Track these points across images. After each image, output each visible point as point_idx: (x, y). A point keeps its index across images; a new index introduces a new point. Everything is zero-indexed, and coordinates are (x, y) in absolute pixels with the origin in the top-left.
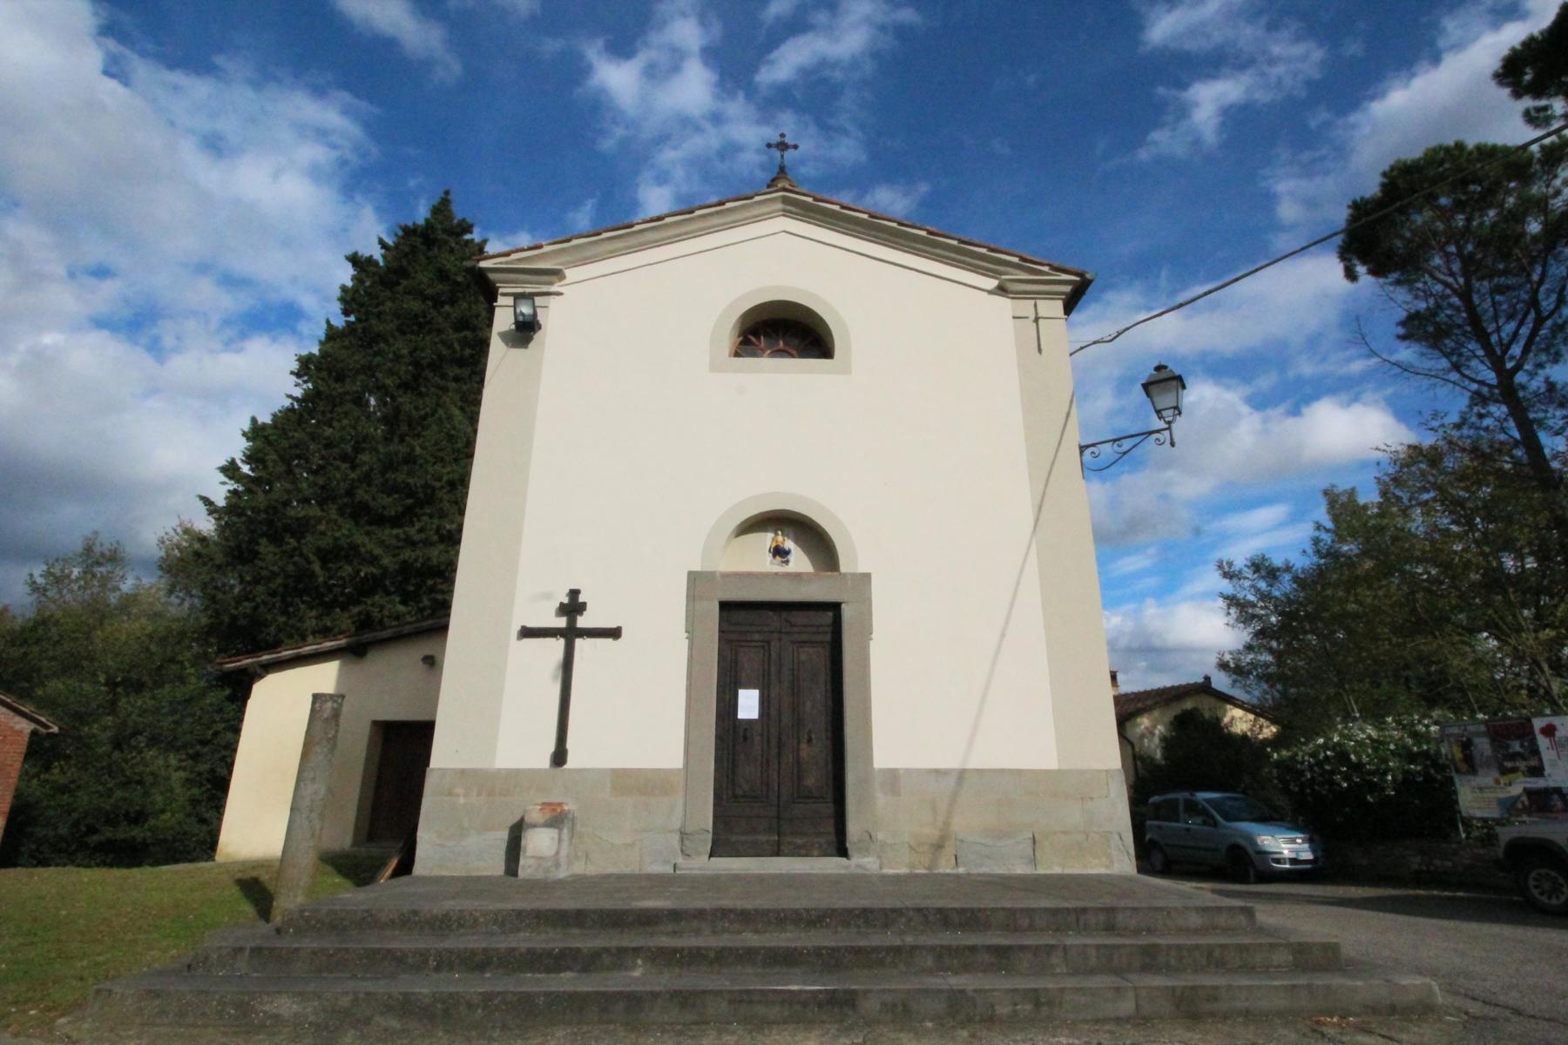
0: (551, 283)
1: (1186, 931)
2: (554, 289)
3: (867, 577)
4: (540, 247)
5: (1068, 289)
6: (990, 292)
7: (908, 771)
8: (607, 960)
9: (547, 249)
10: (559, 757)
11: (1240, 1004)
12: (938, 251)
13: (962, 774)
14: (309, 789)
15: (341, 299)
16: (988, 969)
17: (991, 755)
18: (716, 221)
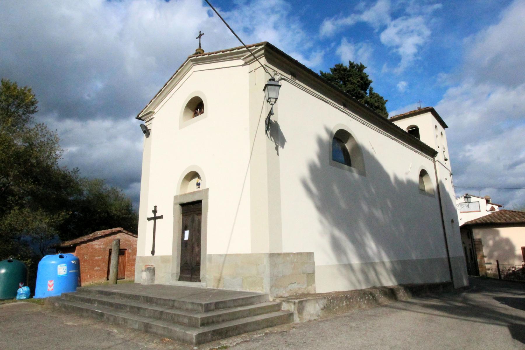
0: (152, 116)
1: (187, 310)
2: (152, 117)
3: (207, 190)
4: (147, 106)
5: (263, 51)
6: (243, 65)
7: (214, 255)
8: (213, 307)
9: (149, 106)
10: (153, 253)
11: (155, 330)
12: (228, 57)
13: (226, 255)
14: (198, 259)
15: (336, 66)
16: (132, 312)
17: (233, 251)
18: (179, 77)
